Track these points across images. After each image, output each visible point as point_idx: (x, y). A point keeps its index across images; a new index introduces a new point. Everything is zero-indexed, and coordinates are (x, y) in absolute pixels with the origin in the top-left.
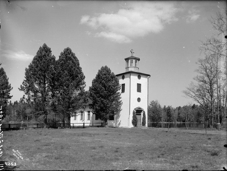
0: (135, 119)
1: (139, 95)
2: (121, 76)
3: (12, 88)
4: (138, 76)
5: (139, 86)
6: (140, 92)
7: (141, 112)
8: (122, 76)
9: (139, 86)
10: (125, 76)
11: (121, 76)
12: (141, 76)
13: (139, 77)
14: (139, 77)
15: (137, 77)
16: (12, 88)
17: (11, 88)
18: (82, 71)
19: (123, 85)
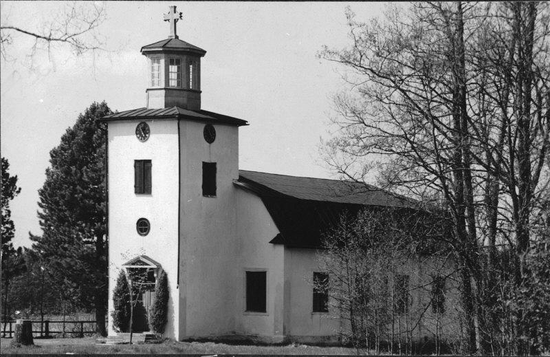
0: (366, 225)
1: (142, 207)
2: (133, 126)
3: (20, 189)
4: (138, 132)
5: (143, 172)
6: (205, 164)
7: (83, 256)
8: (136, 124)
9: (143, 172)
10: (152, 125)
11: (133, 126)
12: (148, 123)
13: (143, 133)
14: (143, 133)
15: (135, 136)
16: (20, 189)
17: (17, 189)
18: (42, 188)
19: (320, 303)
